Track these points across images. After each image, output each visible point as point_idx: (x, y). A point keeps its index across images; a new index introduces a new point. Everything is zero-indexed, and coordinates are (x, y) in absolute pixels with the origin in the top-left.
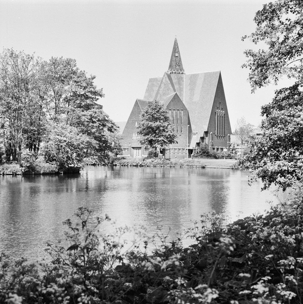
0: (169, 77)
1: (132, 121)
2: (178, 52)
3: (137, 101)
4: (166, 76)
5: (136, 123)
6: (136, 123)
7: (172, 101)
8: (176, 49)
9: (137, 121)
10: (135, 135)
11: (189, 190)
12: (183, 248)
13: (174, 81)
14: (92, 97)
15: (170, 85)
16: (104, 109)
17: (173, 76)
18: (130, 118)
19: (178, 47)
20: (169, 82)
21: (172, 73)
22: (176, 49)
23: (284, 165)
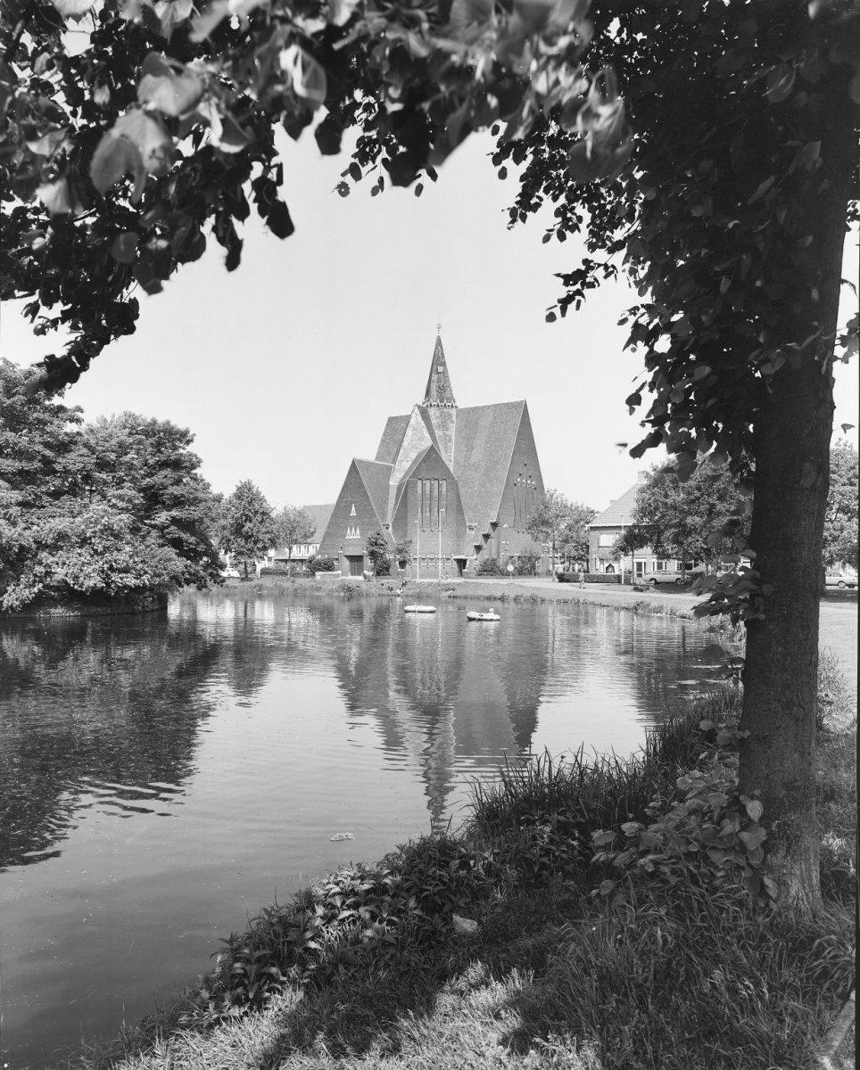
0: (424, 413)
1: (346, 502)
2: (444, 364)
3: (353, 462)
4: (417, 410)
5: (353, 507)
6: (353, 507)
7: (424, 461)
8: (439, 360)
9: (354, 503)
10: (351, 530)
11: (516, 599)
12: (170, 596)
13: (434, 422)
14: (351, 31)
15: (425, 431)
16: (513, 205)
17: (433, 412)
18: (341, 497)
19: (443, 354)
20: (423, 424)
21: (431, 406)
22: (439, 360)
23: (224, 584)
